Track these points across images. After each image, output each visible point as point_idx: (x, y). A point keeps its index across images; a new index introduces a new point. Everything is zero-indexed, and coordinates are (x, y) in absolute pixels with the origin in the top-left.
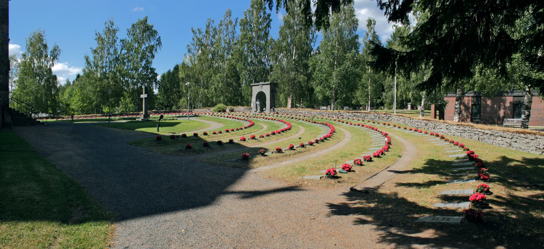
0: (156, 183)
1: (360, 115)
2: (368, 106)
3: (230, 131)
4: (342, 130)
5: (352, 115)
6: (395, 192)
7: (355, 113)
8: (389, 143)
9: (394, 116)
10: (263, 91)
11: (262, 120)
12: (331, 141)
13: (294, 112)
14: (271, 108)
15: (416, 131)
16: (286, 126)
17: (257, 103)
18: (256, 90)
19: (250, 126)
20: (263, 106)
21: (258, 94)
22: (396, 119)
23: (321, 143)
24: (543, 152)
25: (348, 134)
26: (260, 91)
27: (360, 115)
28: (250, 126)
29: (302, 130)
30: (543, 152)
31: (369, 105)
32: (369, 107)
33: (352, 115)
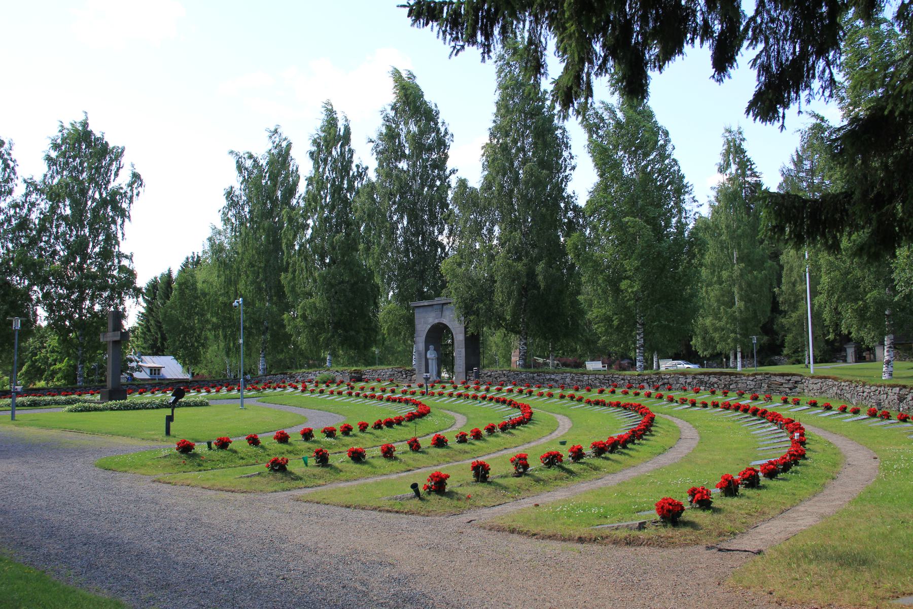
0: (134, 591)
1: (715, 380)
2: (736, 358)
3: (338, 433)
4: (678, 422)
5: (695, 381)
6: (652, 112)
7: (702, 377)
8: (802, 442)
9: (811, 381)
10: (445, 321)
11: (445, 400)
12: (640, 450)
13: (533, 378)
14: (468, 368)
15: (873, 414)
16: (517, 414)
17: (428, 356)
18: (425, 322)
19: (411, 417)
20: (445, 361)
21: (429, 331)
22: (815, 387)
23: (749, 492)
24: (44, 607)
25: (689, 432)
26: (437, 321)
27: (715, 380)
28: (411, 417)
29: (564, 424)
30: (44, 607)
31: (739, 355)
32: (739, 359)
33: (695, 381)
